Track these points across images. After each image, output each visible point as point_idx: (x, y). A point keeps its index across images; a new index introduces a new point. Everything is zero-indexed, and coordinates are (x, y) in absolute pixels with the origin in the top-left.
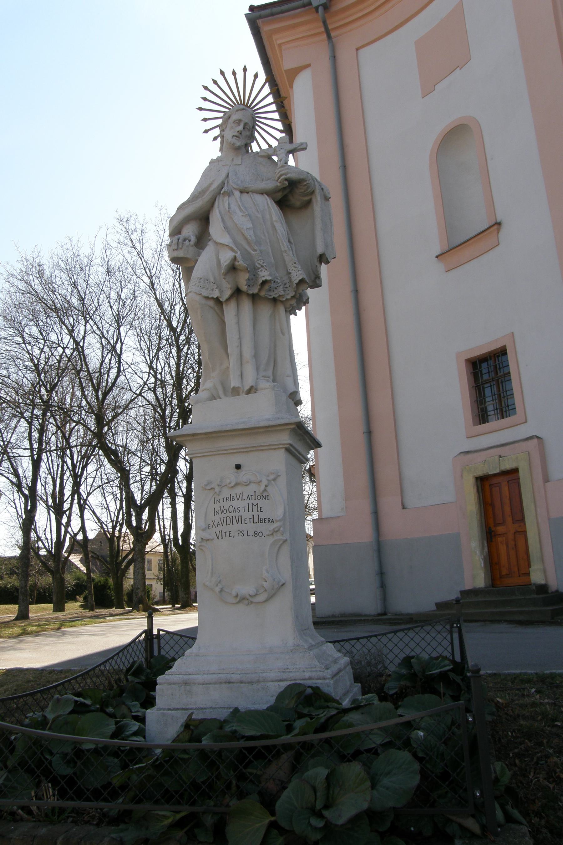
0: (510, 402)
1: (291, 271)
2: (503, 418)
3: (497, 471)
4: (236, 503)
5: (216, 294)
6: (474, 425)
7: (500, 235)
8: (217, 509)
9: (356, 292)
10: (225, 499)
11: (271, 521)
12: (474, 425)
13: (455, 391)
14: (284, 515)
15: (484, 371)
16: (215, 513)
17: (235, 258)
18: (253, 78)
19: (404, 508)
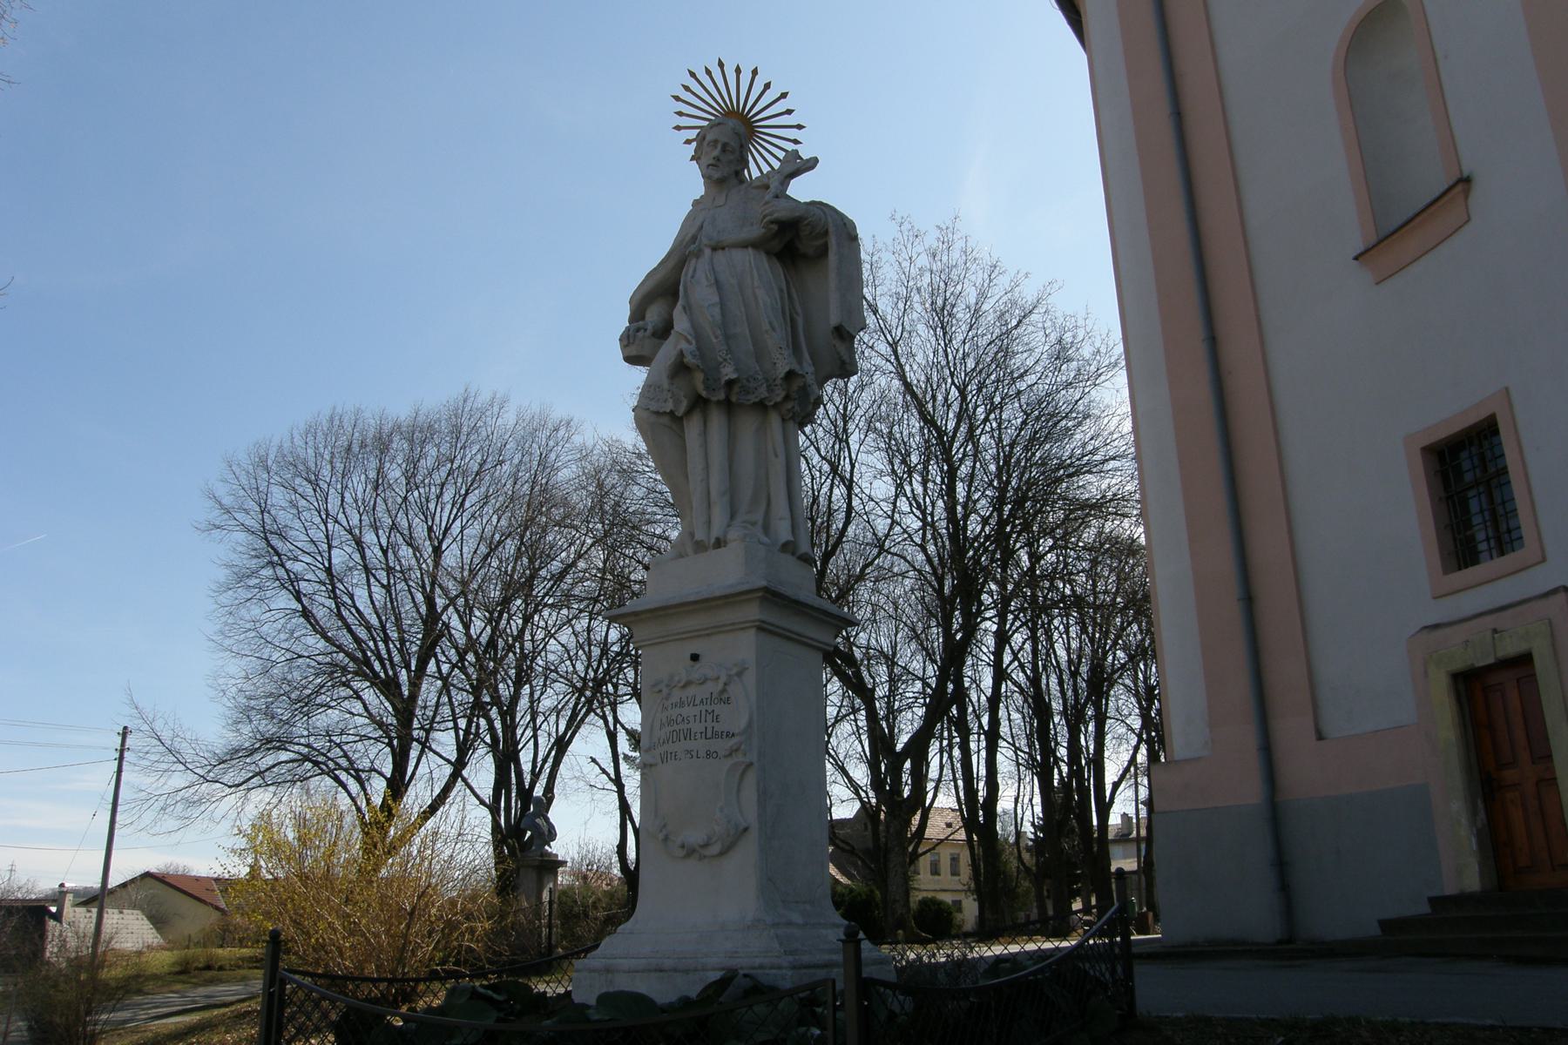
0: (1512, 524)
2: (1502, 553)
3: (1491, 660)
5: (669, 407)
6: (1446, 572)
7: (1471, 200)
9: (1213, 341)
11: (730, 735)
12: (1446, 572)
13: (1404, 512)
14: (750, 725)
15: (1466, 465)
17: (681, 354)
19: (1320, 737)
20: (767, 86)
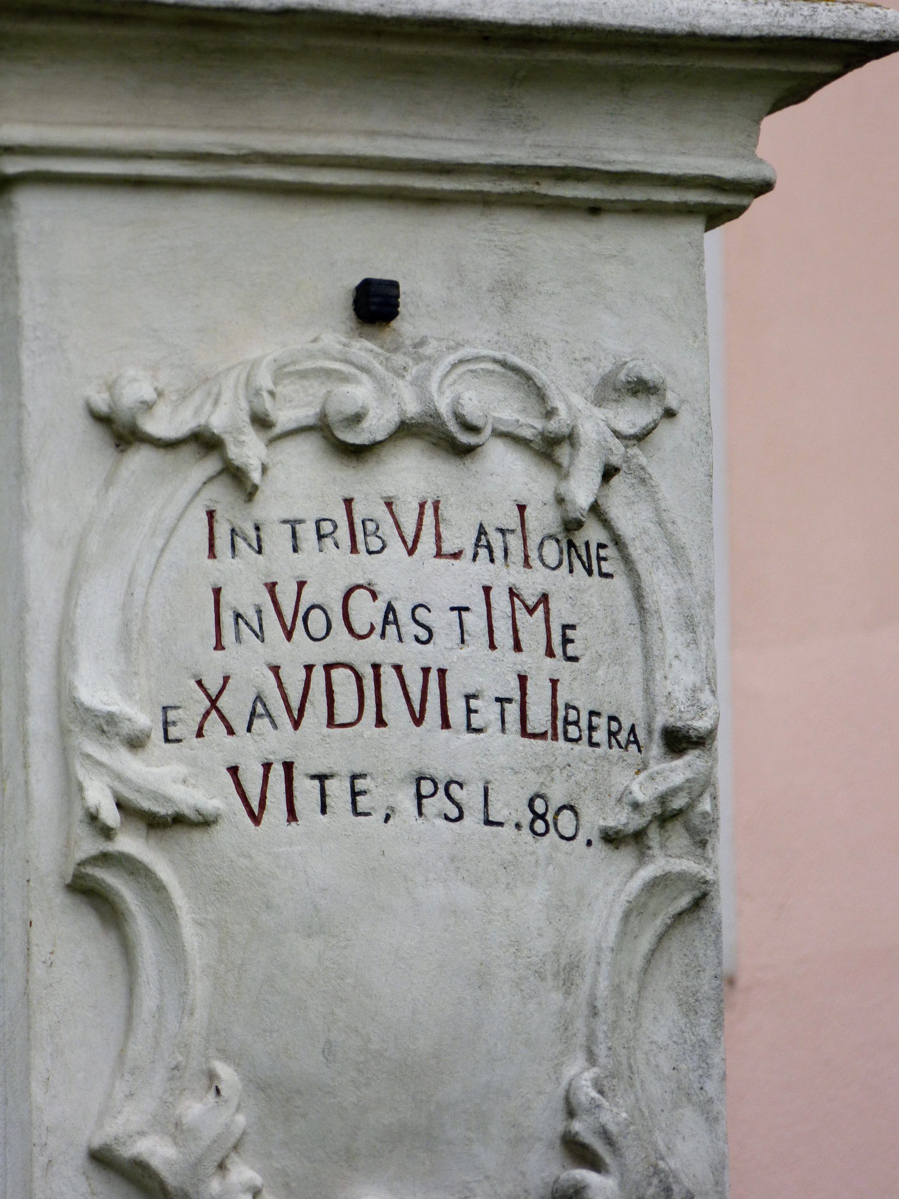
4: (398, 574)
8: (245, 595)
10: (307, 532)
16: (224, 622)
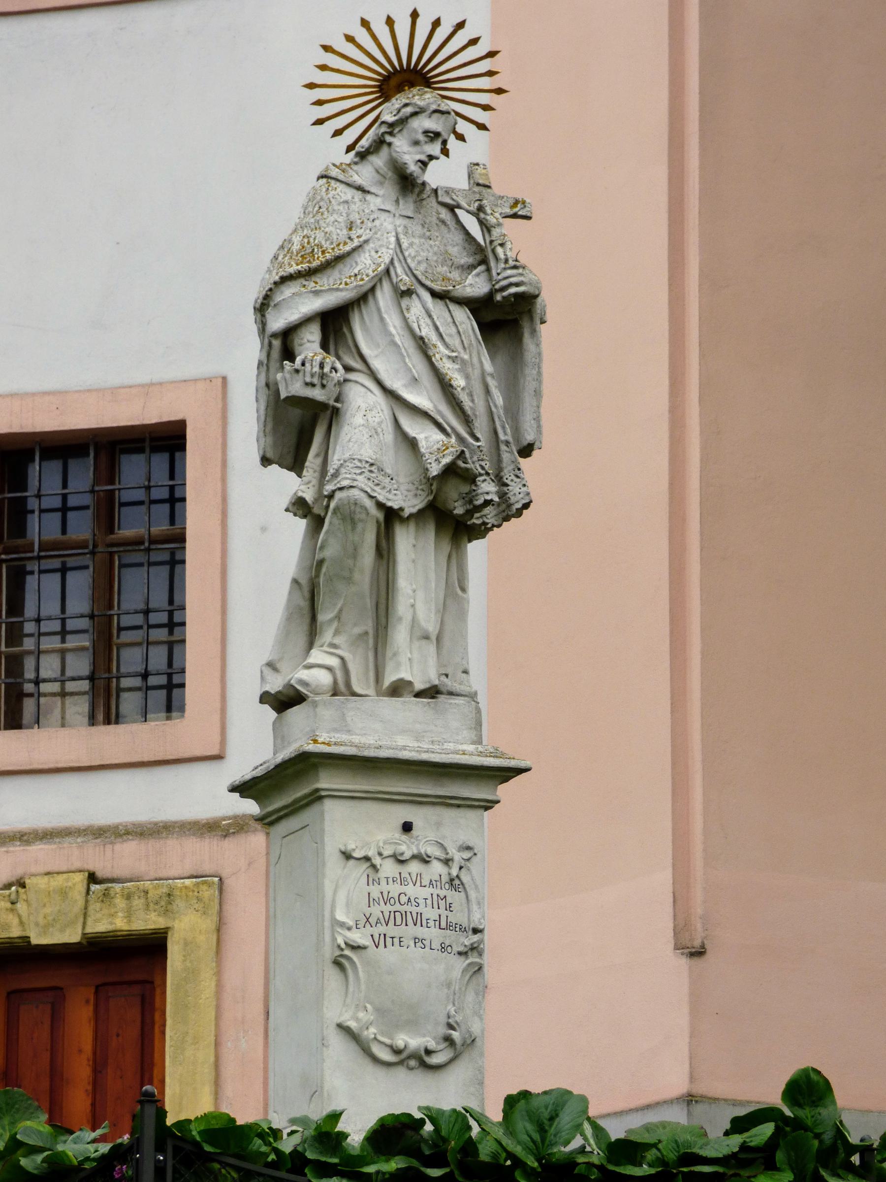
1: (508, 482)
3: (72, 936)
4: (411, 890)
8: (375, 894)
10: (390, 880)
16: (371, 901)
18: (409, 20)
20: (390, 22)
